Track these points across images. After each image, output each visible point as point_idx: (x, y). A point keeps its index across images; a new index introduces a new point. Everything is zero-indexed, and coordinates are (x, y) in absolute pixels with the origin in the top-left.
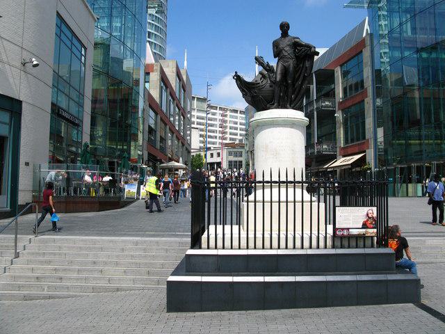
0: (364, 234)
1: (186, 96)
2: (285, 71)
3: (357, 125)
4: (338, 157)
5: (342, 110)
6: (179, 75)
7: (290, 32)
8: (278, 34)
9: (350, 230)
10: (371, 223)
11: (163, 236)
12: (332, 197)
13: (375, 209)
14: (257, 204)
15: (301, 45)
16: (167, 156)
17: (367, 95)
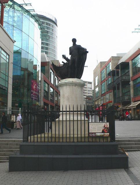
8: (71, 44)
9: (96, 134)
12: (47, 122)
13: (108, 124)
14: (64, 122)
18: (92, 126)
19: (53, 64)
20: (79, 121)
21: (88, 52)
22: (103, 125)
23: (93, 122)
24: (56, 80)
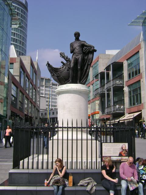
0: (120, 160)
1: (37, 78)
2: (76, 61)
3: (137, 95)
4: (125, 114)
5: (128, 86)
6: (32, 64)
7: (80, 38)
8: (74, 39)
9: (112, 158)
10: (125, 153)
11: (6, 161)
13: (127, 144)
15: (86, 46)
16: (24, 113)
17: (142, 77)
18: (106, 148)
19: (48, 65)
20: (55, 140)
21: (95, 51)
22: (121, 147)
23: (111, 142)
24: (27, 82)
